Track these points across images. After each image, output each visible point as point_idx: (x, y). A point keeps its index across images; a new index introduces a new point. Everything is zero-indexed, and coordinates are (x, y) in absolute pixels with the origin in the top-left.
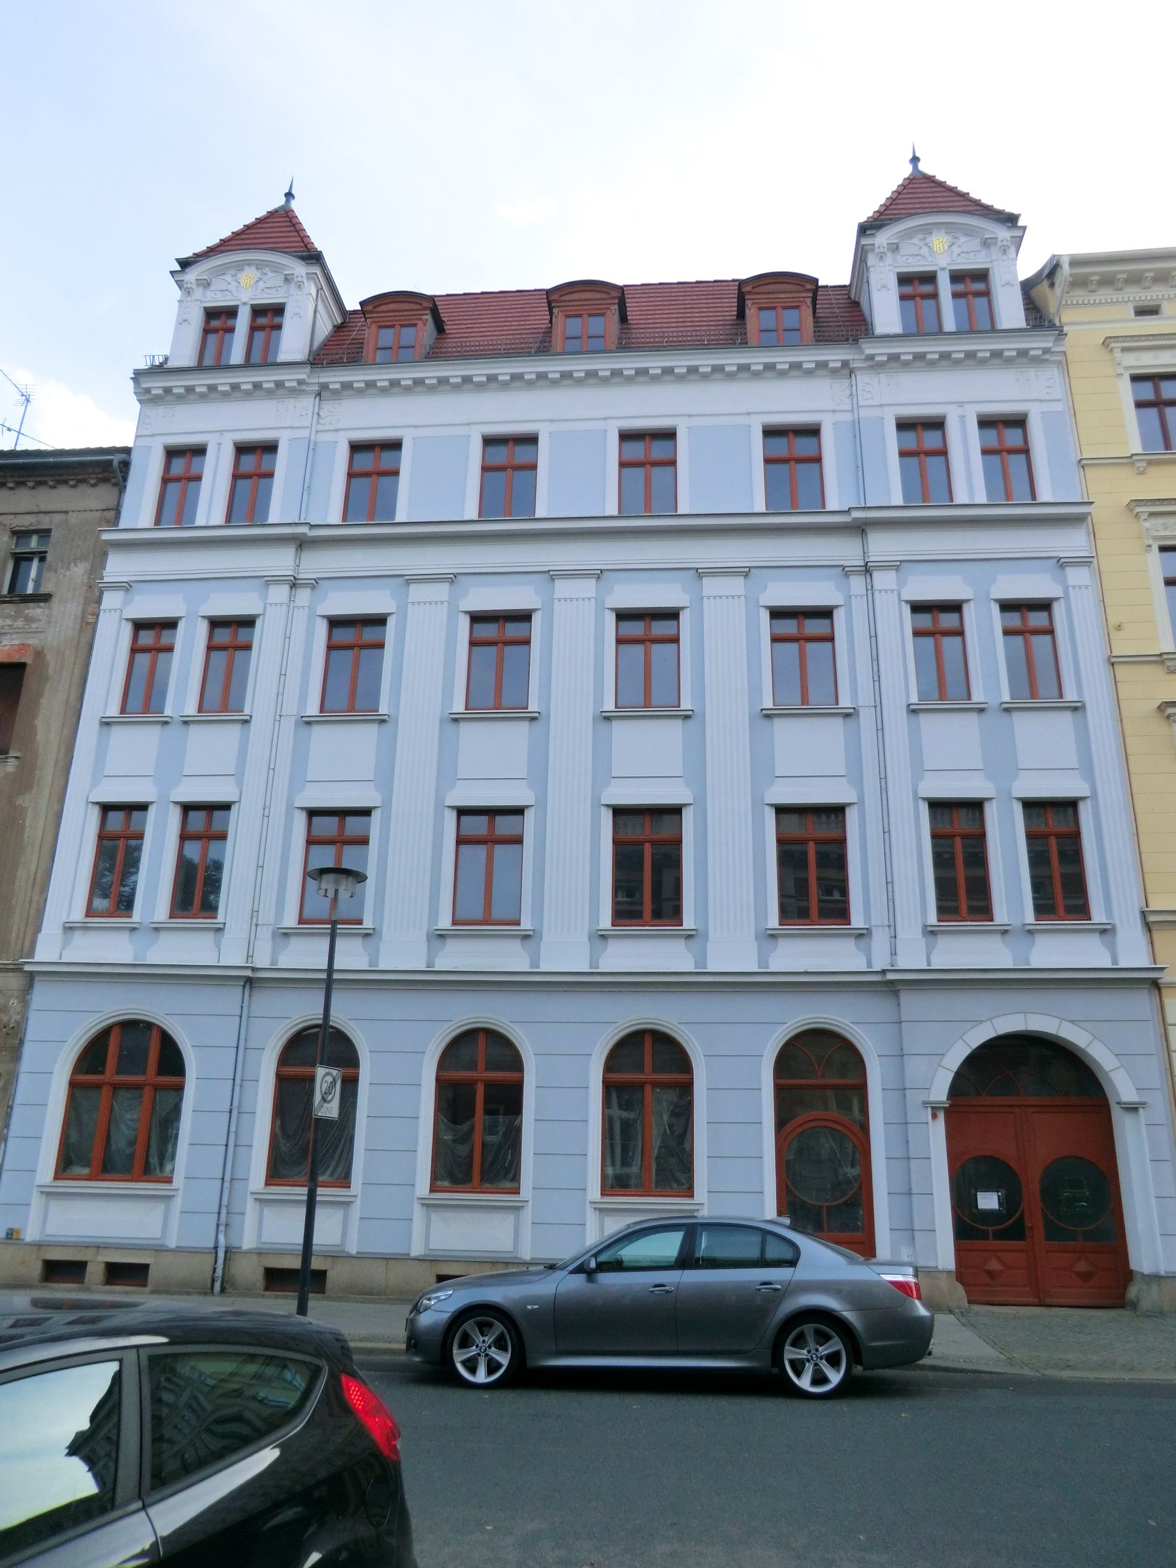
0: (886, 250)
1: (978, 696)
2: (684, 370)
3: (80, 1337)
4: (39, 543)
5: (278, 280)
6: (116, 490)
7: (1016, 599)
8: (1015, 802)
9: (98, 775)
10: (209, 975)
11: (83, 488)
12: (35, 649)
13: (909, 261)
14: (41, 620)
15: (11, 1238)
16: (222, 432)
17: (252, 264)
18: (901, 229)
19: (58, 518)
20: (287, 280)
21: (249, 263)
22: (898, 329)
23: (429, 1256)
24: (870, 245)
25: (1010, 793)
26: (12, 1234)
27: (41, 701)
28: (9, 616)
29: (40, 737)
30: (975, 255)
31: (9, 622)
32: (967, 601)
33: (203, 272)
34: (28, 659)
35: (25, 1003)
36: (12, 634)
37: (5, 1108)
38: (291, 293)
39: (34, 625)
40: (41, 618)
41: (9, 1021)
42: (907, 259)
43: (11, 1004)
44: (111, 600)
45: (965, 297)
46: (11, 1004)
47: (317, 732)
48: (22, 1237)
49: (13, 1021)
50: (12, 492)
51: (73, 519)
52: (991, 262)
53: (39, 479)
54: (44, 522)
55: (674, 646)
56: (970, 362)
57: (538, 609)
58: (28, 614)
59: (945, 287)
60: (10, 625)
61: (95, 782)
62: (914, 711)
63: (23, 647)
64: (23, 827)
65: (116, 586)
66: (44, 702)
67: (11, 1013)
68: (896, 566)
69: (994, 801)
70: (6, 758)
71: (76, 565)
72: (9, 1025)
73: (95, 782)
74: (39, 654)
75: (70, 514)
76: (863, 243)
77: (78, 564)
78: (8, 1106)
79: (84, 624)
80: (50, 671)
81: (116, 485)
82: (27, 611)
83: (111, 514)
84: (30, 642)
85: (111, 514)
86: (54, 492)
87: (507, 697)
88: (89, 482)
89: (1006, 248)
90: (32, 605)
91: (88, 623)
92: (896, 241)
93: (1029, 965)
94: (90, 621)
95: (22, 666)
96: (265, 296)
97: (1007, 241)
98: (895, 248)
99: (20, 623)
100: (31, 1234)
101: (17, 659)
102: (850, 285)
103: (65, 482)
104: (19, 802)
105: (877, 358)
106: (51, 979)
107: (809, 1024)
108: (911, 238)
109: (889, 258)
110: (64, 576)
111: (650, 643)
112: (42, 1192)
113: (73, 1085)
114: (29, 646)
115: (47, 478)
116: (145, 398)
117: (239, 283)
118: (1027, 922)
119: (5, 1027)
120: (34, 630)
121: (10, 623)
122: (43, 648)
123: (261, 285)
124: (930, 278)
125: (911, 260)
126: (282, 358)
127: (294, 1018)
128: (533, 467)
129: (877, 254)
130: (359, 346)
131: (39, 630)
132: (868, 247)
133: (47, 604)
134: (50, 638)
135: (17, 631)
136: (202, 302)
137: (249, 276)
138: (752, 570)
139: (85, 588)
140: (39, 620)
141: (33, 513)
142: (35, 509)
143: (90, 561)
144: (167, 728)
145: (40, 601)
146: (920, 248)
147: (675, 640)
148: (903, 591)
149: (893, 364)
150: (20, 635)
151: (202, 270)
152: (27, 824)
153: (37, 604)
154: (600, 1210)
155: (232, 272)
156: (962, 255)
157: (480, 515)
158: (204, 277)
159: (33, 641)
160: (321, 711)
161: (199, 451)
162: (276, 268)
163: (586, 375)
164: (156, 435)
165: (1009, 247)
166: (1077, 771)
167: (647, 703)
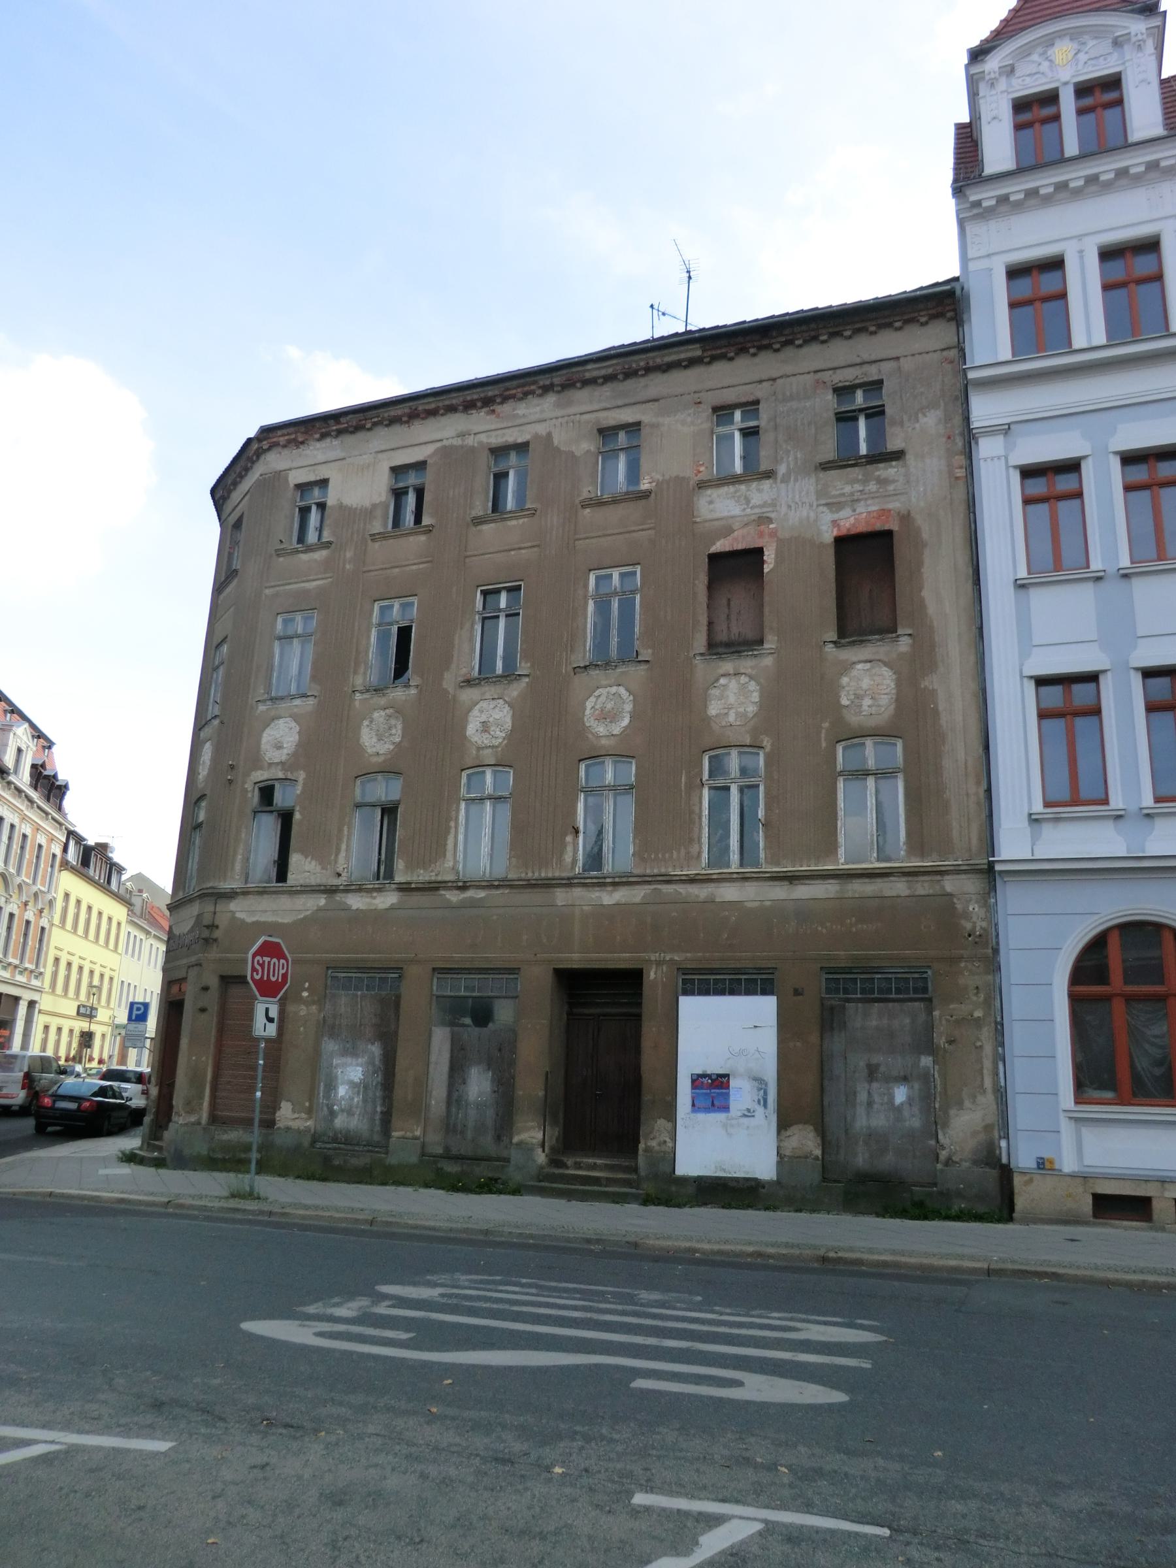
0: (1145, 36)
1: (1096, 564)
2: (1081, 183)
3: (1076, 1279)
4: (865, 399)
5: (1105, 46)
6: (953, 325)
7: (1067, 459)
8: (1132, 672)
9: (1026, 642)
10: (1111, 868)
11: (789, 352)
12: (899, 513)
13: (1026, 83)
14: (897, 481)
15: (1043, 1169)
16: (1080, 237)
17: (1065, 35)
18: (1007, 52)
19: (887, 367)
20: (1117, 43)
21: (1060, 35)
22: (1159, 131)
23: (1082, 1173)
24: (1127, 34)
25: (1127, 662)
26: (1043, 1163)
27: (922, 570)
28: (857, 481)
29: (932, 609)
30: (1105, 59)
31: (858, 487)
32: (1085, 457)
33: (1004, 58)
34: (894, 526)
35: (991, 910)
36: (866, 499)
37: (993, 1025)
38: (1128, 57)
39: (891, 488)
40: (896, 478)
41: (974, 927)
42: (1023, 80)
43: (971, 909)
44: (987, 448)
45: (1094, 111)
46: (971, 909)
47: (1036, 595)
48: (1057, 1167)
49: (978, 928)
50: (825, 346)
51: (907, 364)
52: (1123, 63)
53: (858, 326)
54: (873, 373)
55: (1077, 502)
56: (1032, 202)
57: (1087, 456)
58: (879, 476)
59: (1068, 104)
60: (861, 491)
61: (1024, 654)
62: (1023, 586)
63: (884, 512)
64: (936, 712)
65: (991, 431)
66: (927, 571)
67: (974, 919)
68: (1006, 430)
69: (1109, 673)
70: (898, 636)
71: (925, 416)
72: (975, 932)
73: (1024, 654)
74: (906, 518)
75: (901, 360)
76: (971, 72)
77: (928, 414)
78: (996, 1023)
79: (953, 479)
80: (925, 536)
81: (950, 320)
82: (877, 473)
83: (953, 353)
84: (890, 506)
85: (953, 353)
86: (875, 339)
87: (1070, 554)
88: (918, 321)
89: (1141, 43)
90: (881, 465)
91: (957, 478)
92: (1011, 62)
93: (1144, 853)
94: (958, 475)
95: (889, 534)
96: (1090, 69)
97: (1142, 34)
98: (1010, 71)
99: (872, 487)
100: (1068, 1165)
101: (878, 526)
102: (971, 122)
103: (889, 325)
104: (925, 683)
105: (985, 204)
106: (1098, 877)
107: (1111, 919)
108: (1029, 55)
109: (1002, 84)
110: (914, 429)
111: (1157, 487)
112: (1070, 1118)
113: (1075, 999)
114: (890, 511)
115: (868, 324)
116: (971, 214)
117: (1051, 61)
118: (1144, 805)
119: (970, 935)
120: (892, 493)
121: (861, 488)
122: (909, 512)
123: (1082, 57)
124: (1051, 98)
125: (1028, 79)
126: (989, 170)
127: (1102, 915)
128: (1063, 296)
129: (988, 81)
130: (973, 159)
131: (898, 492)
132: (1121, 39)
133: (901, 463)
134: (914, 500)
135: (872, 495)
136: (1009, 93)
137: (1063, 51)
138: (1012, 427)
139: (944, 439)
140: (894, 481)
141: (857, 365)
142: (858, 360)
143: (942, 408)
144: (1101, 584)
145: (892, 459)
146: (1039, 64)
147: (1078, 495)
148: (1010, 458)
149: (1153, 175)
150: (877, 500)
151: (1003, 55)
152: (941, 708)
153: (887, 464)
154: (1077, 1120)
155: (1040, 50)
156: (1089, 62)
157: (1014, 355)
158: (1007, 63)
159: (894, 505)
160: (1029, 574)
161: (1056, 264)
162: (1097, 33)
163: (1025, 196)
164: (993, 254)
165: (1144, 41)
166: (1096, 643)
167: (1058, 566)
